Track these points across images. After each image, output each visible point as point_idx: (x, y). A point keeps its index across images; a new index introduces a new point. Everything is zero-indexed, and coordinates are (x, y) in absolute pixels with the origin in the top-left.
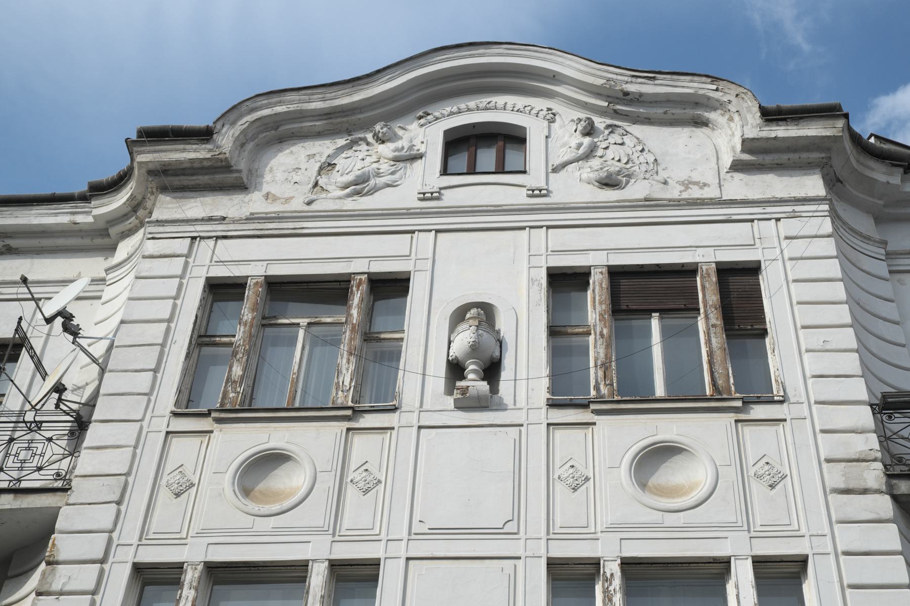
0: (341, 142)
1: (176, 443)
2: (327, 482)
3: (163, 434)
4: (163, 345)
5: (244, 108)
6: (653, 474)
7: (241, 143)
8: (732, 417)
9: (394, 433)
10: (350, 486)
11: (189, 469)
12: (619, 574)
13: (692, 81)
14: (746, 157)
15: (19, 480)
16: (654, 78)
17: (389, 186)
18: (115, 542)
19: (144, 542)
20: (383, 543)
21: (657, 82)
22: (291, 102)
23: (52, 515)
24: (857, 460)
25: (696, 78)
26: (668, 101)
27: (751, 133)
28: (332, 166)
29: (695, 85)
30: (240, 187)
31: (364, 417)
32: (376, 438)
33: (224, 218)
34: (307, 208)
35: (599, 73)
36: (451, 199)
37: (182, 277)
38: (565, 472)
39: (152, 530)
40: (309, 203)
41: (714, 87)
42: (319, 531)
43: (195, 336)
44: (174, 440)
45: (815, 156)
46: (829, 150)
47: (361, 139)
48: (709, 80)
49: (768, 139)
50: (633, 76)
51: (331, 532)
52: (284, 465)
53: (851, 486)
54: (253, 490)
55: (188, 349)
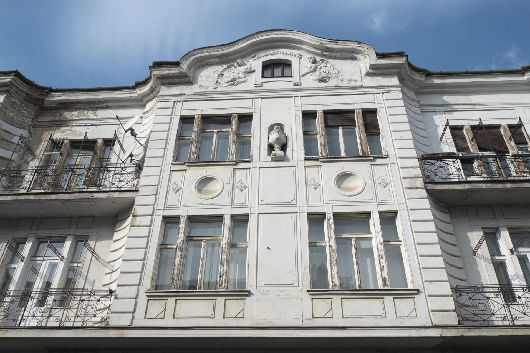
1: (174, 174)
2: (228, 187)
3: (169, 171)
4: (167, 140)
6: (342, 183)
8: (370, 163)
9: (251, 170)
10: (236, 188)
13: (351, 43)
14: (371, 71)
16: (337, 42)
17: (243, 82)
19: (166, 208)
21: (338, 44)
22: (207, 52)
25: (352, 42)
30: (190, 83)
31: (239, 164)
33: (185, 94)
34: (214, 90)
35: (317, 41)
38: (312, 183)
40: (215, 88)
41: (359, 46)
44: (173, 173)
46: (400, 68)
47: (232, 65)
48: (357, 43)
50: (330, 42)
54: (202, 190)
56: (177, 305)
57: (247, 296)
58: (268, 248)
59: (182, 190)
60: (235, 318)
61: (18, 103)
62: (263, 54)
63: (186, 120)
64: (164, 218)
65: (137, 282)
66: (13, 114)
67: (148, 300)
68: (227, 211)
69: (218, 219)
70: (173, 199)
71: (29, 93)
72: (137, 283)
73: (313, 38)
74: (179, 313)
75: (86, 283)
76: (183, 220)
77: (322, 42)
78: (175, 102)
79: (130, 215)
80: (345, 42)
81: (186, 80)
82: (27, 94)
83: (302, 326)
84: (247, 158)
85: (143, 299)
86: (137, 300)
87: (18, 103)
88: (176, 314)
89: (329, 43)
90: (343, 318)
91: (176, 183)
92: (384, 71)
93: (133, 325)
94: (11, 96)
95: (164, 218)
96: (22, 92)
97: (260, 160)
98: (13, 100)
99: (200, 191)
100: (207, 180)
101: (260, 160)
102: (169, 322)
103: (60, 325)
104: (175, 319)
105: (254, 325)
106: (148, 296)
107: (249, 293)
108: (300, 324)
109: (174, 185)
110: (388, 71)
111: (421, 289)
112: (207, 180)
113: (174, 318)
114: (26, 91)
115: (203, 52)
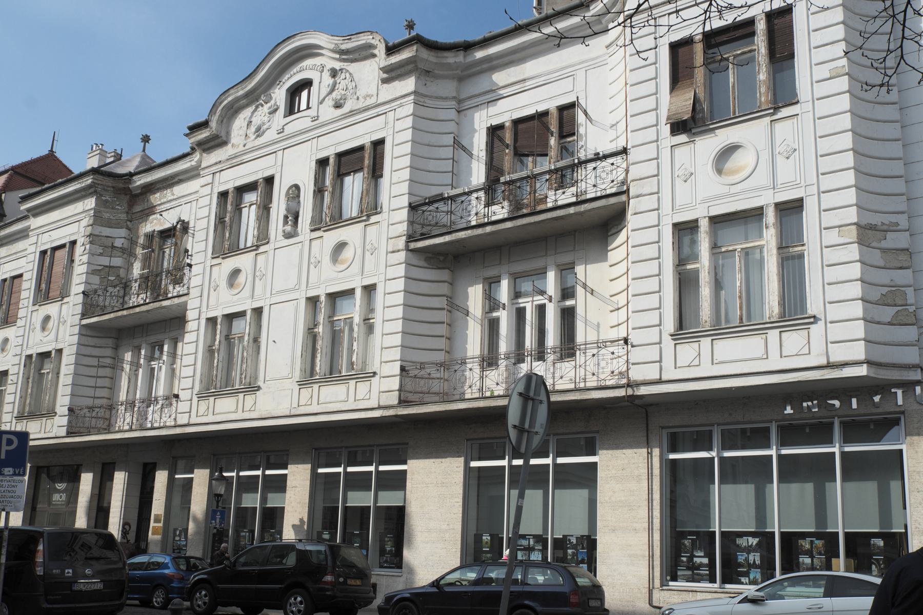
0: (254, 107)
1: (677, 151)
2: (765, 156)
3: (670, 148)
4: (207, 228)
5: (217, 104)
6: (340, 254)
7: (221, 121)
8: (363, 224)
9: (799, 117)
10: (677, 179)
11: (374, 242)
12: (325, 301)
13: (364, 36)
14: (385, 76)
15: (556, 201)
16: (350, 39)
17: (268, 129)
18: (661, 215)
19: (675, 212)
20: (804, 187)
21: (352, 40)
22: (232, 94)
23: (186, 303)
24: (399, 237)
25: (365, 34)
26: (359, 48)
27: (383, 63)
28: (251, 122)
29: (366, 37)
30: (224, 143)
31: (781, 111)
32: (788, 123)
33: (220, 161)
34: (244, 149)
35: (332, 41)
36: (289, 130)
37: (211, 194)
38: (681, 173)
39: (779, 183)
40: (244, 146)
41: (371, 37)
42: (765, 188)
43: (218, 219)
44: (676, 150)
45: (410, 67)
46: (415, 61)
47: (259, 105)
48: (370, 33)
49: (389, 65)
50: (343, 40)
51: (772, 187)
52: (345, 249)
53: (394, 250)
54: (722, 169)
55: (215, 227)
56: (715, 346)
57: (257, 390)
58: (274, 341)
59: (693, 176)
60: (689, 366)
61: (109, 199)
62: (287, 76)
63: (223, 195)
64: (675, 225)
65: (190, 386)
66: (108, 215)
67: (675, 344)
68: (767, 199)
69: (757, 214)
70: (683, 193)
71: (114, 185)
72: (191, 386)
73: (328, 38)
74: (718, 357)
75: (617, 327)
76: (704, 225)
77: (336, 42)
78: (213, 173)
79: (622, 229)
80: (358, 35)
81: (219, 141)
82: (113, 187)
83: (289, 415)
84: (518, 171)
85: (668, 343)
86: (662, 345)
87: (109, 199)
88: (715, 358)
89: (341, 42)
90: (781, 357)
91: (683, 167)
92: (399, 72)
93: (190, 423)
94: (101, 195)
95: (675, 225)
96: (108, 187)
97: (276, 239)
98: (104, 198)
99: (719, 171)
100: (341, 246)
101: (276, 239)
102: (315, 408)
103: (575, 387)
104: (715, 366)
105: (260, 417)
106: (198, 397)
107: (259, 388)
108: (288, 414)
109: (782, 145)
110: (403, 70)
111: (378, 372)
112: (730, 150)
113: (712, 364)
114: (110, 185)
115: (229, 95)
